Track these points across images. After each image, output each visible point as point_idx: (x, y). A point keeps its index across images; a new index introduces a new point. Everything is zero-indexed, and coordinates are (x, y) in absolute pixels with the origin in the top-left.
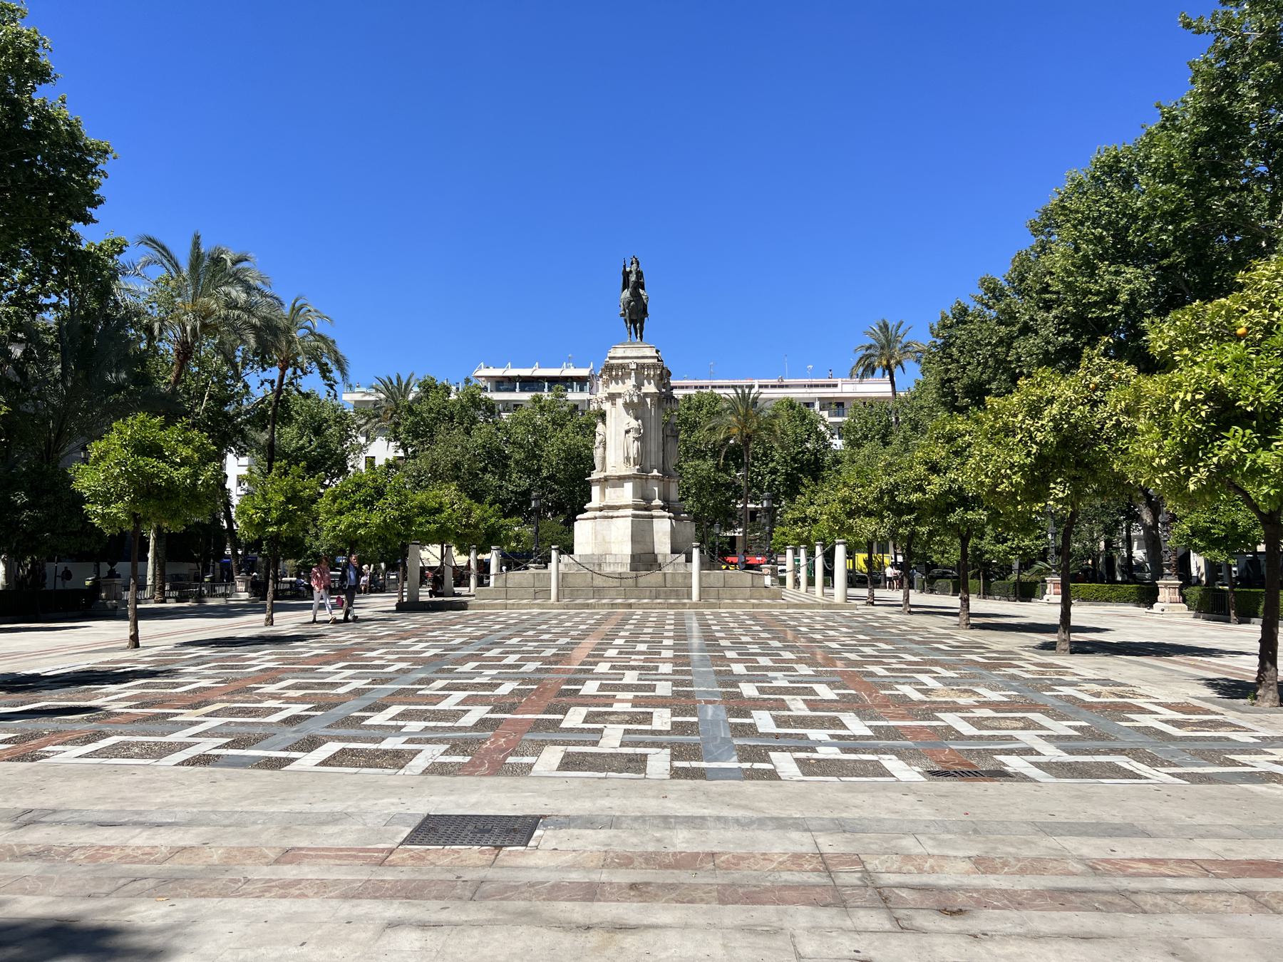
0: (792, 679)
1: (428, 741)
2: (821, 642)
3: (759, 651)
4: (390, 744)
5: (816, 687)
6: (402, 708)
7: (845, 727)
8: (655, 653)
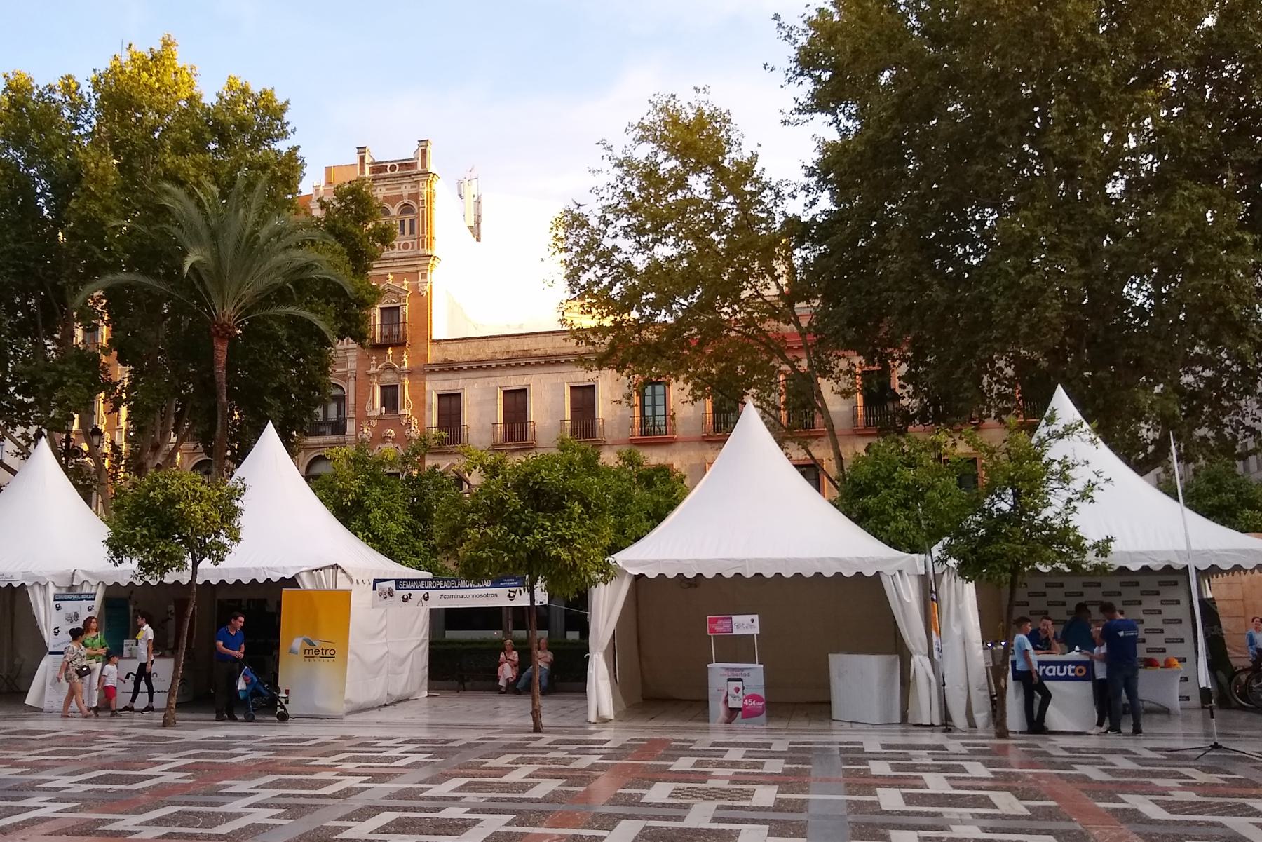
0: (936, 757)
1: (490, 811)
2: (1067, 766)
3: (930, 762)
4: (453, 812)
5: (993, 796)
6: (464, 781)
7: (995, 807)
8: (755, 765)
